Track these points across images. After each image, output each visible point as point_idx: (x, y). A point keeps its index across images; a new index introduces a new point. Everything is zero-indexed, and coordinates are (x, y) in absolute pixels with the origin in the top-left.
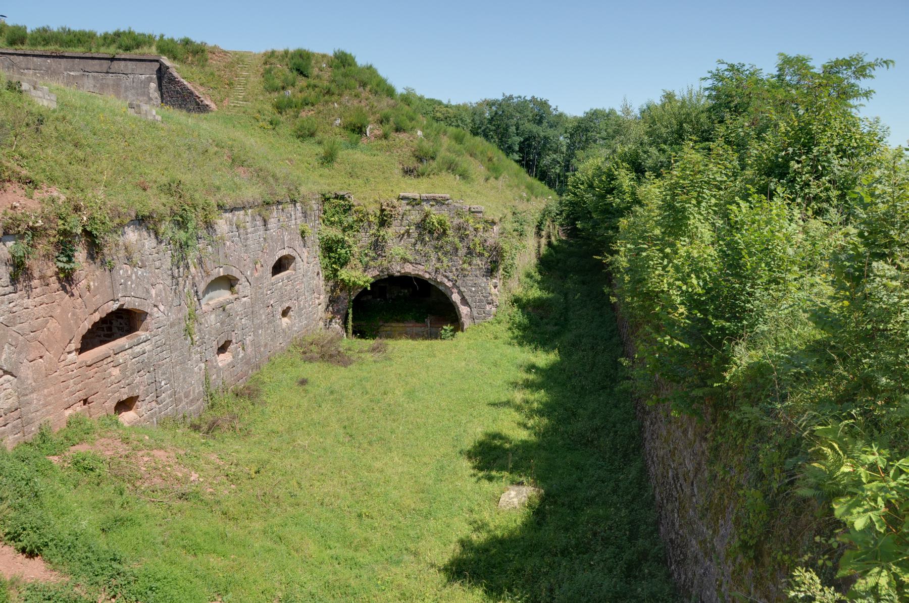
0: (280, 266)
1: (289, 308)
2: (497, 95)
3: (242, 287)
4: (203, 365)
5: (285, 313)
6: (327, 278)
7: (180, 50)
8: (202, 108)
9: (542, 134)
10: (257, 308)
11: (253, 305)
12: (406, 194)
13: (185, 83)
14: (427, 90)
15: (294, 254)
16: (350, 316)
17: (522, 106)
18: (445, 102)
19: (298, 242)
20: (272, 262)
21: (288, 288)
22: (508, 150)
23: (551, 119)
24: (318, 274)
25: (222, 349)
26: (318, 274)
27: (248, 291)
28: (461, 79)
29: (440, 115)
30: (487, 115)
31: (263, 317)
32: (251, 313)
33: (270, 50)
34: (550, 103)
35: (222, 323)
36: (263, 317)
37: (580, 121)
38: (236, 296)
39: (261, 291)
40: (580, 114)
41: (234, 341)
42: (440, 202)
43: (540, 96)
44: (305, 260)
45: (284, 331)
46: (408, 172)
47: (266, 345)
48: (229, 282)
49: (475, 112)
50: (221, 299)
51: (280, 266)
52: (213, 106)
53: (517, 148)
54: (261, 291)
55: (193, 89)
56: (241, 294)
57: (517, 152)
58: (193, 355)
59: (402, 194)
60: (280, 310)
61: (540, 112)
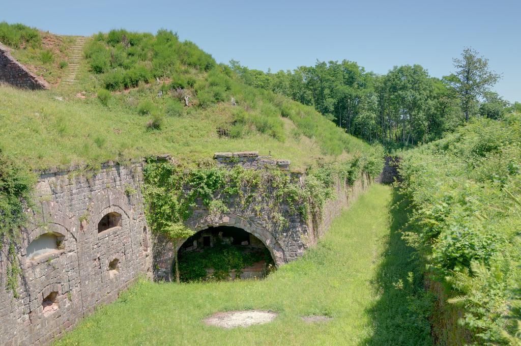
0: (107, 222)
1: (116, 260)
2: (311, 64)
3: (68, 243)
4: (27, 316)
5: (113, 265)
6: (154, 232)
7: (16, 38)
8: (35, 86)
9: (354, 94)
10: (83, 262)
11: (79, 259)
12: (220, 154)
13: (20, 65)
14: (252, 64)
15: (120, 211)
16: (177, 267)
17: (335, 69)
18: (265, 71)
19: (123, 200)
20: (98, 220)
21: (115, 242)
22: (325, 111)
23: (361, 80)
24: (145, 229)
25: (49, 300)
26: (145, 229)
27: (74, 246)
28: (284, 55)
29: (249, 78)
30: (304, 81)
31: (90, 269)
32: (77, 266)
33: (97, 33)
34: (358, 64)
35: (47, 276)
36: (90, 269)
37: (387, 80)
38: (62, 251)
39: (87, 246)
40: (385, 73)
41: (60, 292)
42: (251, 159)
43: (351, 59)
44: (131, 217)
45: (112, 282)
46: (222, 133)
47: (93, 295)
48: (57, 240)
49: (294, 80)
50: (47, 254)
51: (107, 222)
52: (46, 84)
53: (332, 108)
54: (87, 246)
55: (27, 71)
56: (67, 249)
57: (332, 113)
58: (16, 307)
59: (217, 154)
60: (107, 262)
61: (351, 76)
